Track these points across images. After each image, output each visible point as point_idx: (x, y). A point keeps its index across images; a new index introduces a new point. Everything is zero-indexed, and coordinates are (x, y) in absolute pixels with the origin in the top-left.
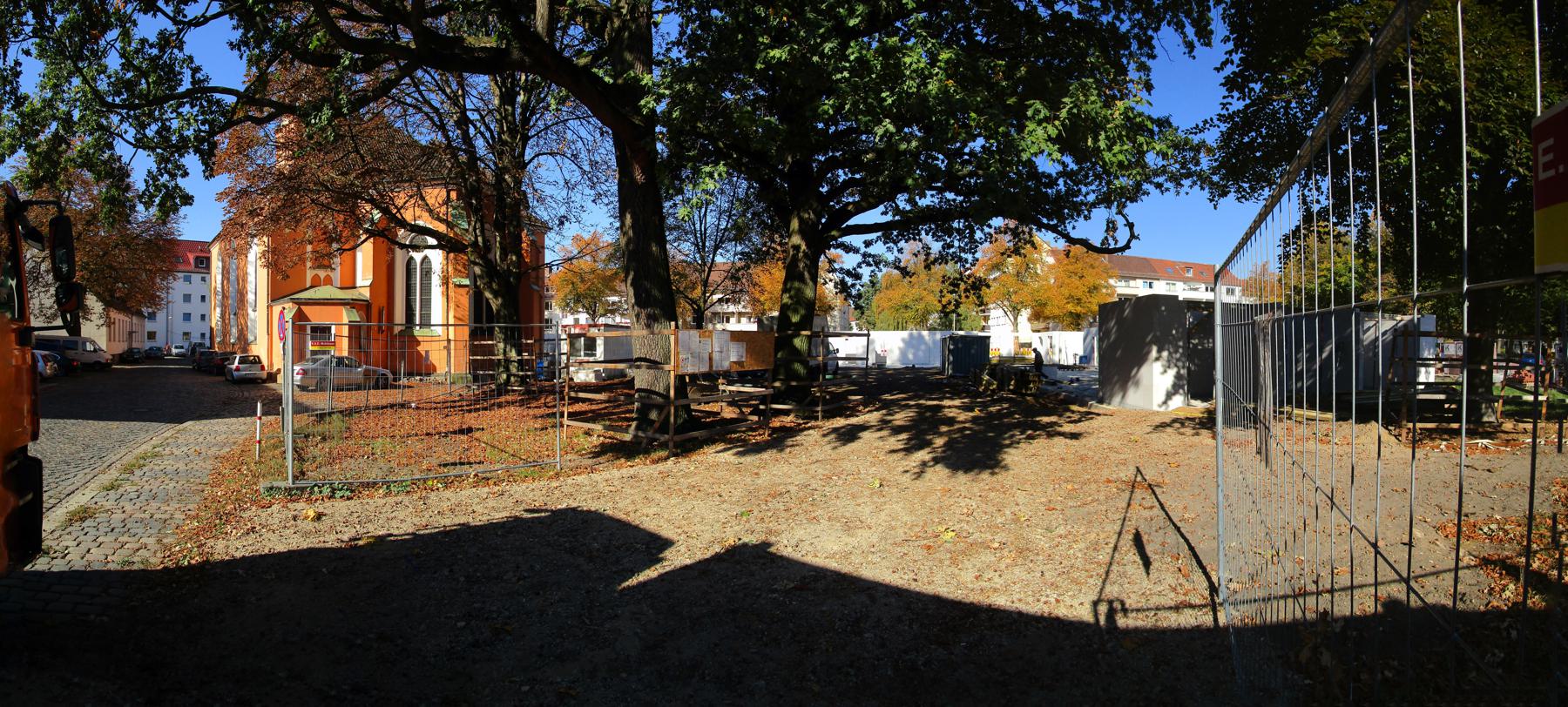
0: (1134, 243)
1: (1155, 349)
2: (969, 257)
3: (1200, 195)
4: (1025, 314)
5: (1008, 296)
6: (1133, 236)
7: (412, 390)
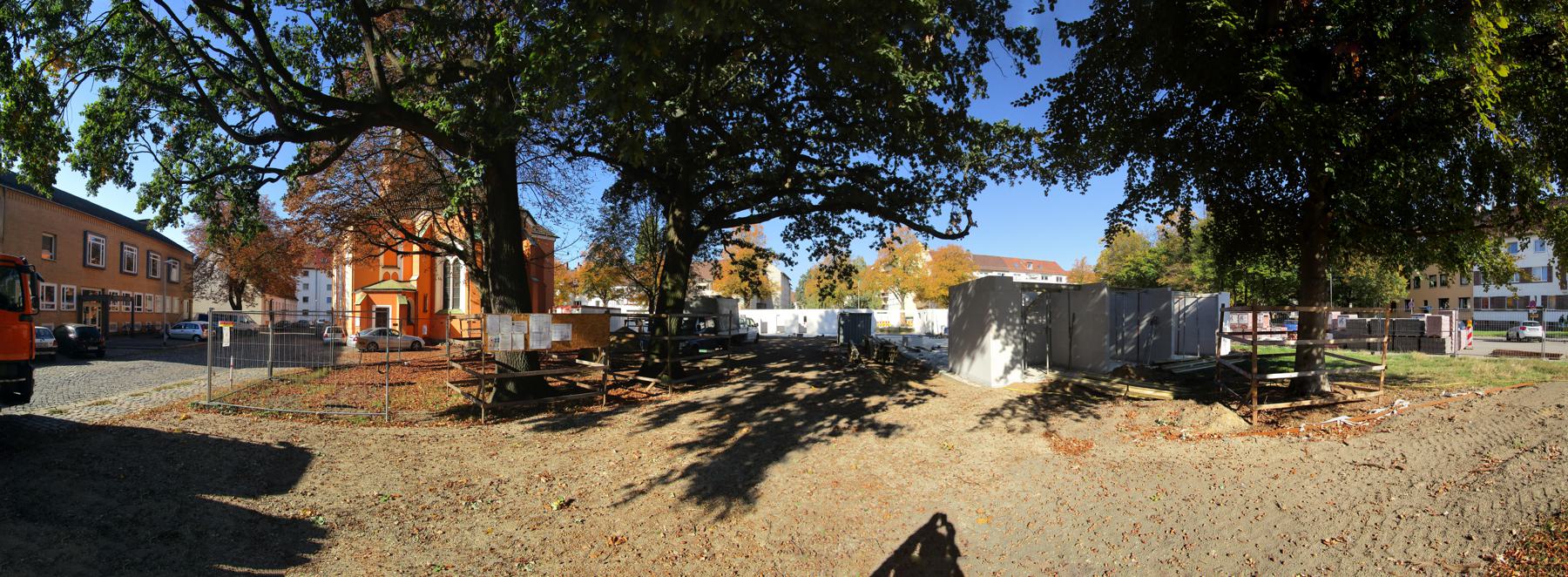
0: (972, 229)
1: (994, 327)
2: (844, 250)
3: (1029, 186)
4: (910, 297)
5: (898, 284)
6: (971, 224)
7: (440, 353)
